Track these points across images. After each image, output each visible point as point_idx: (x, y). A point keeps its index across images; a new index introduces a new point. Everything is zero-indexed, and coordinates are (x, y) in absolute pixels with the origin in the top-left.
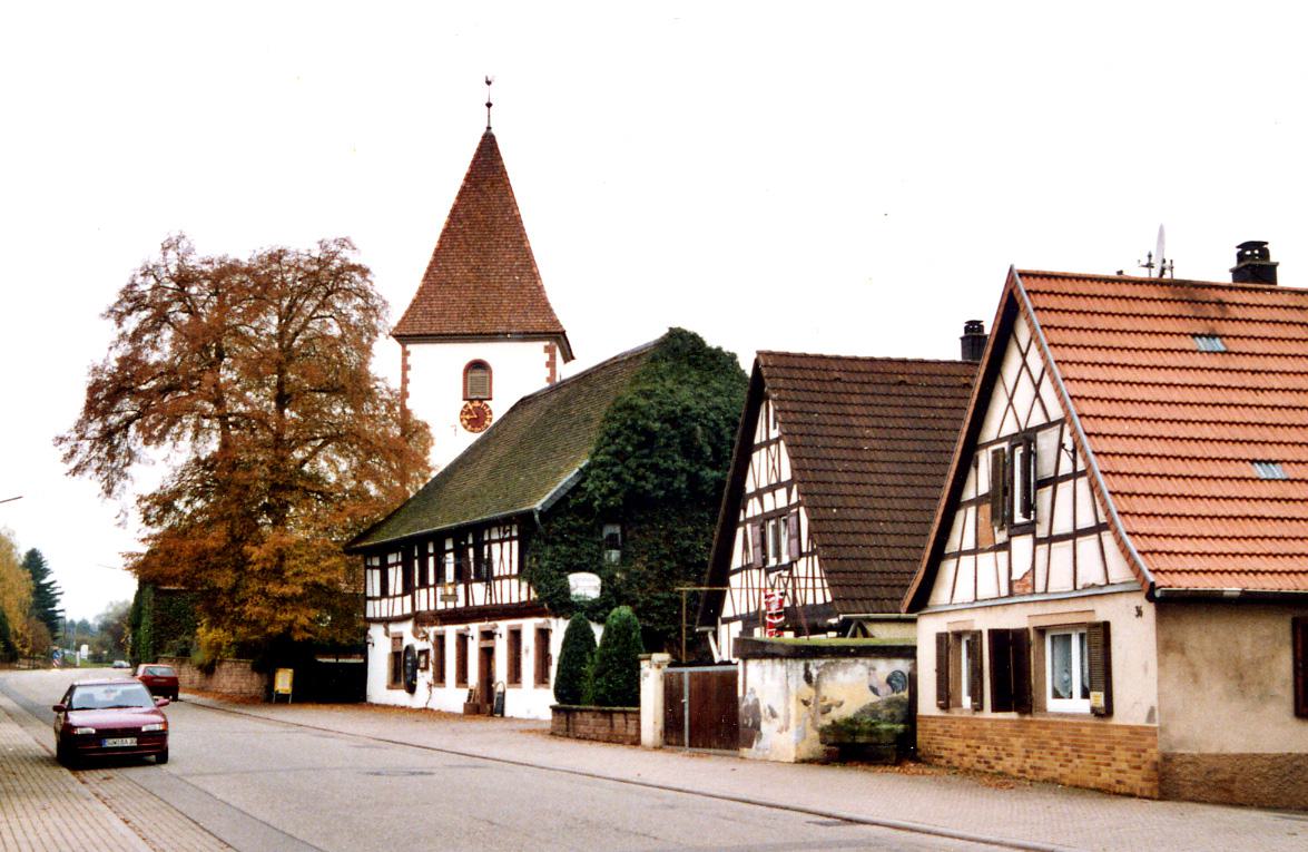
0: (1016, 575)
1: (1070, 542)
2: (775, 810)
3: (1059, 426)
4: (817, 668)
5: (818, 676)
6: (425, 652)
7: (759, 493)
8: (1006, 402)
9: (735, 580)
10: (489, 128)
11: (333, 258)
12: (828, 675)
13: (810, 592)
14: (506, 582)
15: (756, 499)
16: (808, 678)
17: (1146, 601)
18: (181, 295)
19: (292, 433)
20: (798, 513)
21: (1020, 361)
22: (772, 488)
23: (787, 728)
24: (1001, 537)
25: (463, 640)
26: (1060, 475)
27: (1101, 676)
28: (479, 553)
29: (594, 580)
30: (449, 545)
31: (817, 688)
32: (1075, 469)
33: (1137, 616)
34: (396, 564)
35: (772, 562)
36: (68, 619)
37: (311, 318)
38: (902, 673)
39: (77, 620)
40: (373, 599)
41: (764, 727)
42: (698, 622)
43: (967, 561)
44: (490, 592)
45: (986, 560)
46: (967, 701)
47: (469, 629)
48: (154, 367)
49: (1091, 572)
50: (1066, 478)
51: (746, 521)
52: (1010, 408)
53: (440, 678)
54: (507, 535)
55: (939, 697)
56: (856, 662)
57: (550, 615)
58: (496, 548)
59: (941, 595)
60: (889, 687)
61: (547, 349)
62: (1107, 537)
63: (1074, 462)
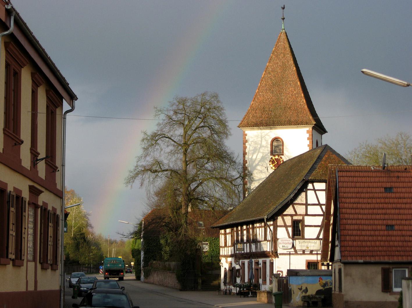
2: (205, 305)
28: (253, 232)
34: (229, 233)
40: (222, 247)
58: (258, 229)
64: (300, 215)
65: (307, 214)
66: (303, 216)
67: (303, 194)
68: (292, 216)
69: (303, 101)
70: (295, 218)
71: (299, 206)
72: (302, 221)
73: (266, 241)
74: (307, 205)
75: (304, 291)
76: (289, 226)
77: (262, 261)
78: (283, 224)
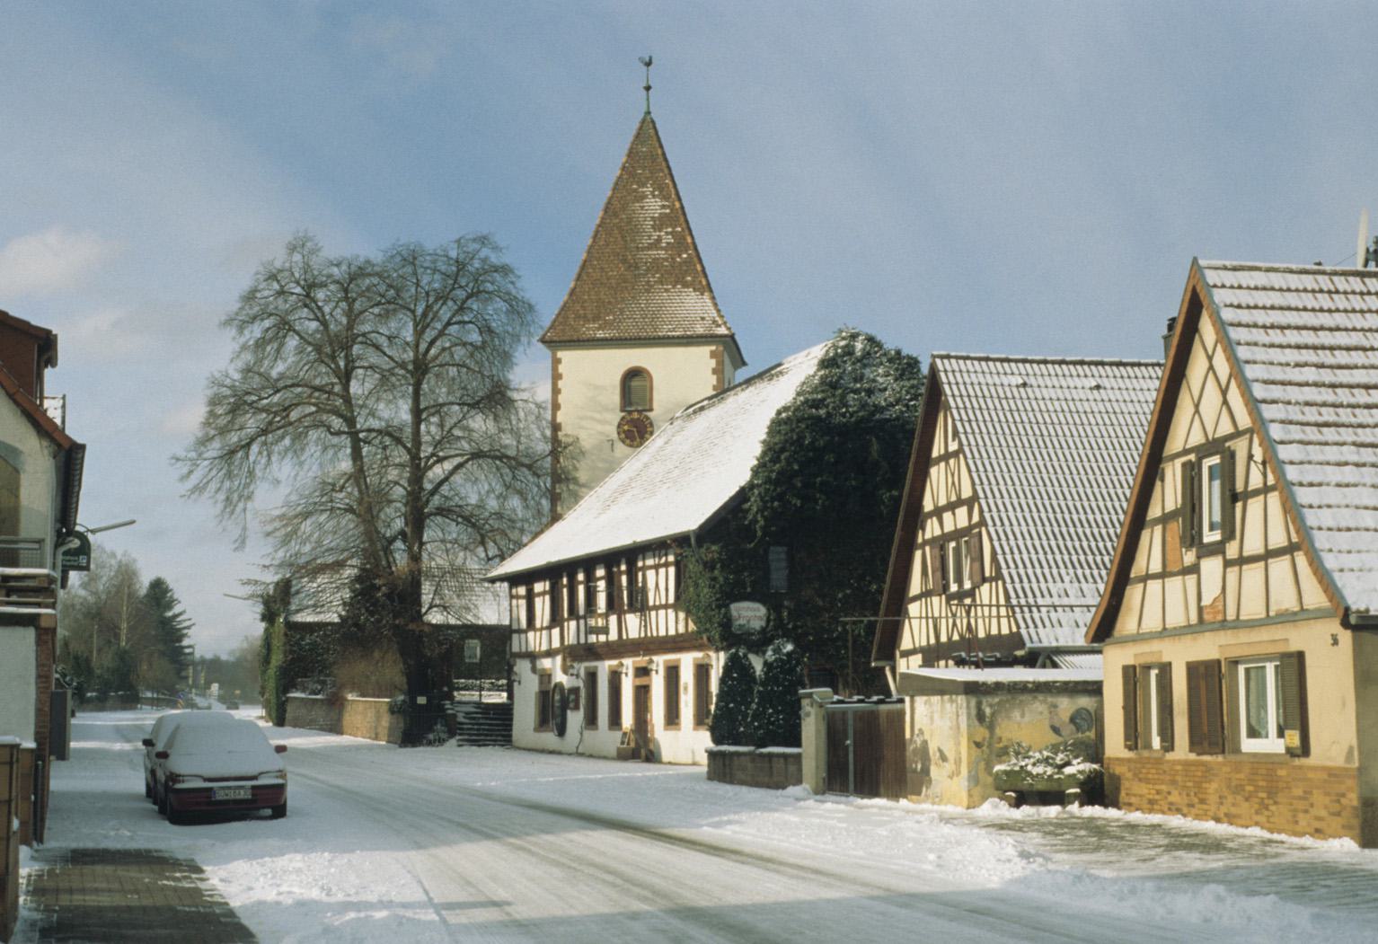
0: (1206, 601)
1: (1262, 564)
3: (1248, 436)
4: (991, 706)
5: (993, 714)
6: (575, 691)
7: (938, 512)
8: (1192, 410)
9: (914, 609)
11: (472, 259)
12: (1003, 714)
13: (994, 621)
14: (662, 612)
15: (935, 519)
16: (980, 717)
17: (1341, 629)
18: (308, 300)
19: (430, 450)
20: (980, 533)
21: (1206, 364)
22: (952, 507)
23: (959, 773)
24: (1189, 557)
25: (615, 679)
26: (1250, 489)
27: (1296, 713)
29: (759, 610)
30: (581, 577)
31: (991, 728)
32: (1265, 483)
33: (1333, 645)
34: (543, 594)
35: (954, 588)
36: (197, 655)
37: (449, 324)
38: (1087, 711)
39: (209, 656)
41: (934, 772)
42: (873, 655)
43: (1154, 586)
44: (645, 624)
45: (1174, 583)
46: (1156, 742)
47: (622, 665)
48: (278, 380)
49: (1285, 599)
50: (1256, 493)
51: (925, 542)
52: (1197, 416)
53: (591, 720)
54: (663, 560)
55: (1127, 738)
56: (1036, 697)
57: (709, 649)
58: (651, 574)
59: (1127, 624)
60: (1072, 727)
61: (713, 355)
62: (1301, 559)
63: (1265, 475)
69: (700, 282)
77: (586, 668)
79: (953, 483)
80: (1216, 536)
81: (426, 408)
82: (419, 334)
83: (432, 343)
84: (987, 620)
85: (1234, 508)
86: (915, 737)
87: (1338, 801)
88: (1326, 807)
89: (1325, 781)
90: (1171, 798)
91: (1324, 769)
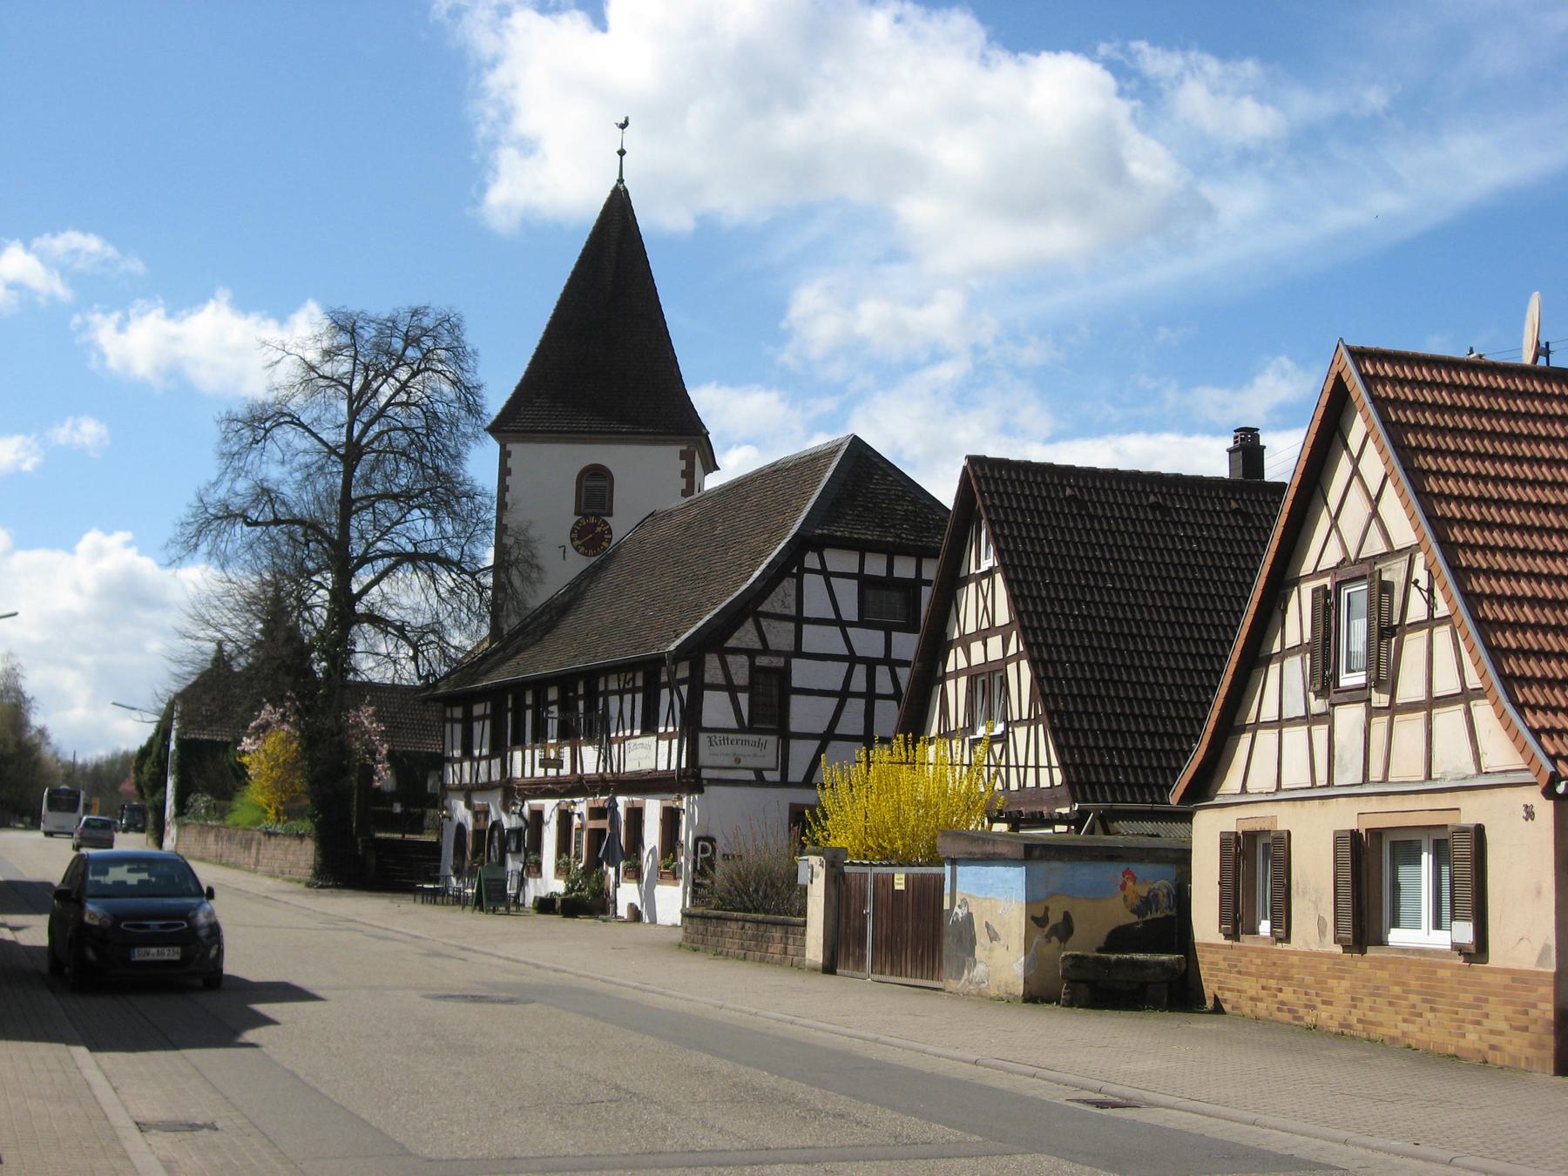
6: (1165, 802)
10: (621, 180)
13: (1031, 772)
15: (959, 649)
34: (483, 718)
44: (606, 757)
50: (1417, 626)
58: (614, 701)
61: (683, 455)
64: (778, 653)
65: (798, 653)
66: (788, 656)
67: (788, 585)
68: (751, 654)
70: (762, 661)
71: (776, 624)
72: (784, 674)
73: (655, 738)
74: (799, 620)
75: (1054, 930)
76: (743, 689)
78: (721, 680)
79: (985, 607)
80: (1359, 679)
81: (359, 499)
82: (353, 415)
83: (367, 426)
84: (1022, 770)
85: (444, 727)
86: (956, 909)
87: (1526, 1013)
88: (1507, 1019)
89: (1506, 987)
90: (1281, 996)
91: (1507, 971)
